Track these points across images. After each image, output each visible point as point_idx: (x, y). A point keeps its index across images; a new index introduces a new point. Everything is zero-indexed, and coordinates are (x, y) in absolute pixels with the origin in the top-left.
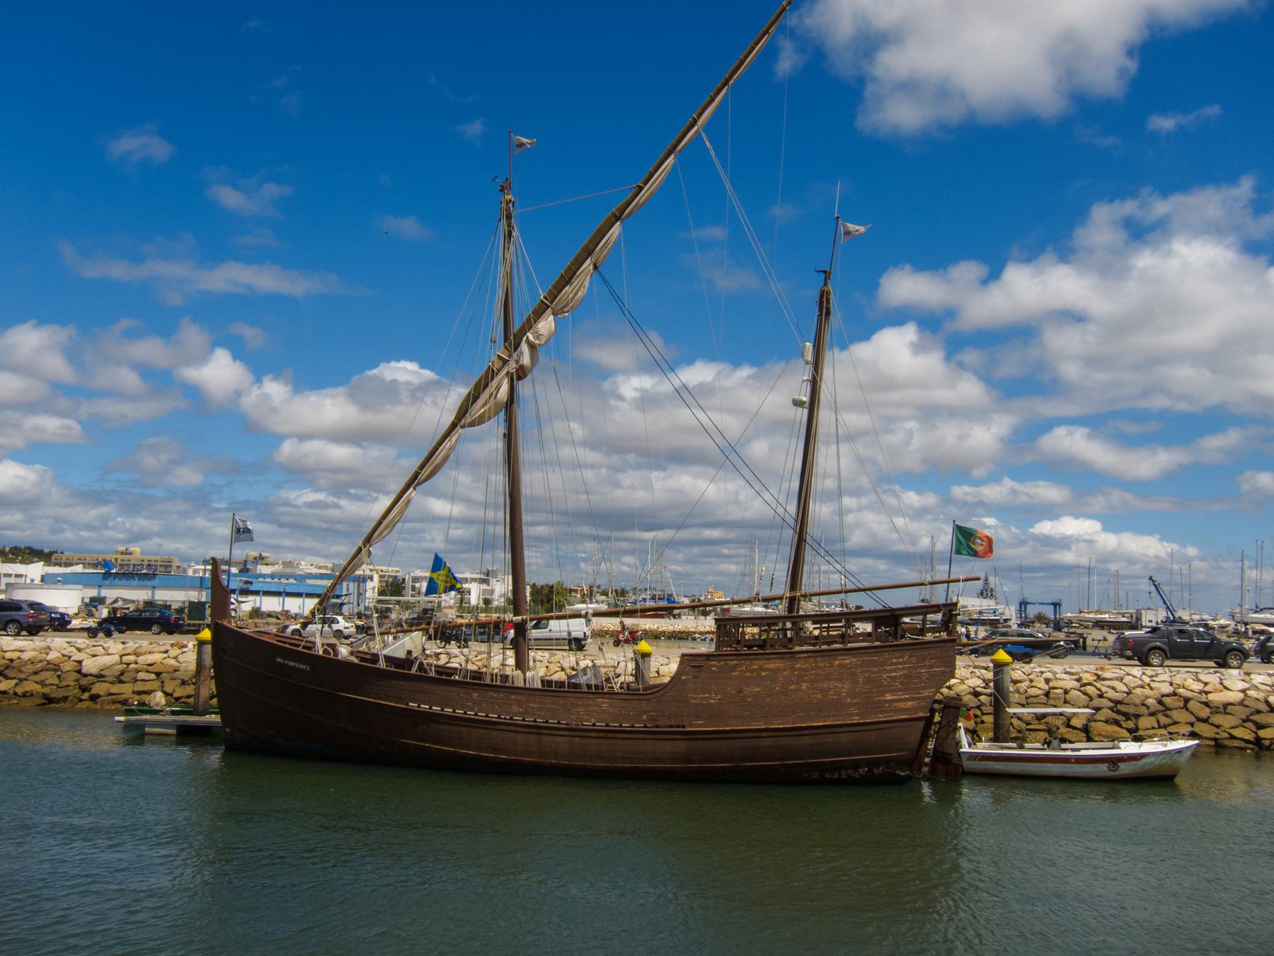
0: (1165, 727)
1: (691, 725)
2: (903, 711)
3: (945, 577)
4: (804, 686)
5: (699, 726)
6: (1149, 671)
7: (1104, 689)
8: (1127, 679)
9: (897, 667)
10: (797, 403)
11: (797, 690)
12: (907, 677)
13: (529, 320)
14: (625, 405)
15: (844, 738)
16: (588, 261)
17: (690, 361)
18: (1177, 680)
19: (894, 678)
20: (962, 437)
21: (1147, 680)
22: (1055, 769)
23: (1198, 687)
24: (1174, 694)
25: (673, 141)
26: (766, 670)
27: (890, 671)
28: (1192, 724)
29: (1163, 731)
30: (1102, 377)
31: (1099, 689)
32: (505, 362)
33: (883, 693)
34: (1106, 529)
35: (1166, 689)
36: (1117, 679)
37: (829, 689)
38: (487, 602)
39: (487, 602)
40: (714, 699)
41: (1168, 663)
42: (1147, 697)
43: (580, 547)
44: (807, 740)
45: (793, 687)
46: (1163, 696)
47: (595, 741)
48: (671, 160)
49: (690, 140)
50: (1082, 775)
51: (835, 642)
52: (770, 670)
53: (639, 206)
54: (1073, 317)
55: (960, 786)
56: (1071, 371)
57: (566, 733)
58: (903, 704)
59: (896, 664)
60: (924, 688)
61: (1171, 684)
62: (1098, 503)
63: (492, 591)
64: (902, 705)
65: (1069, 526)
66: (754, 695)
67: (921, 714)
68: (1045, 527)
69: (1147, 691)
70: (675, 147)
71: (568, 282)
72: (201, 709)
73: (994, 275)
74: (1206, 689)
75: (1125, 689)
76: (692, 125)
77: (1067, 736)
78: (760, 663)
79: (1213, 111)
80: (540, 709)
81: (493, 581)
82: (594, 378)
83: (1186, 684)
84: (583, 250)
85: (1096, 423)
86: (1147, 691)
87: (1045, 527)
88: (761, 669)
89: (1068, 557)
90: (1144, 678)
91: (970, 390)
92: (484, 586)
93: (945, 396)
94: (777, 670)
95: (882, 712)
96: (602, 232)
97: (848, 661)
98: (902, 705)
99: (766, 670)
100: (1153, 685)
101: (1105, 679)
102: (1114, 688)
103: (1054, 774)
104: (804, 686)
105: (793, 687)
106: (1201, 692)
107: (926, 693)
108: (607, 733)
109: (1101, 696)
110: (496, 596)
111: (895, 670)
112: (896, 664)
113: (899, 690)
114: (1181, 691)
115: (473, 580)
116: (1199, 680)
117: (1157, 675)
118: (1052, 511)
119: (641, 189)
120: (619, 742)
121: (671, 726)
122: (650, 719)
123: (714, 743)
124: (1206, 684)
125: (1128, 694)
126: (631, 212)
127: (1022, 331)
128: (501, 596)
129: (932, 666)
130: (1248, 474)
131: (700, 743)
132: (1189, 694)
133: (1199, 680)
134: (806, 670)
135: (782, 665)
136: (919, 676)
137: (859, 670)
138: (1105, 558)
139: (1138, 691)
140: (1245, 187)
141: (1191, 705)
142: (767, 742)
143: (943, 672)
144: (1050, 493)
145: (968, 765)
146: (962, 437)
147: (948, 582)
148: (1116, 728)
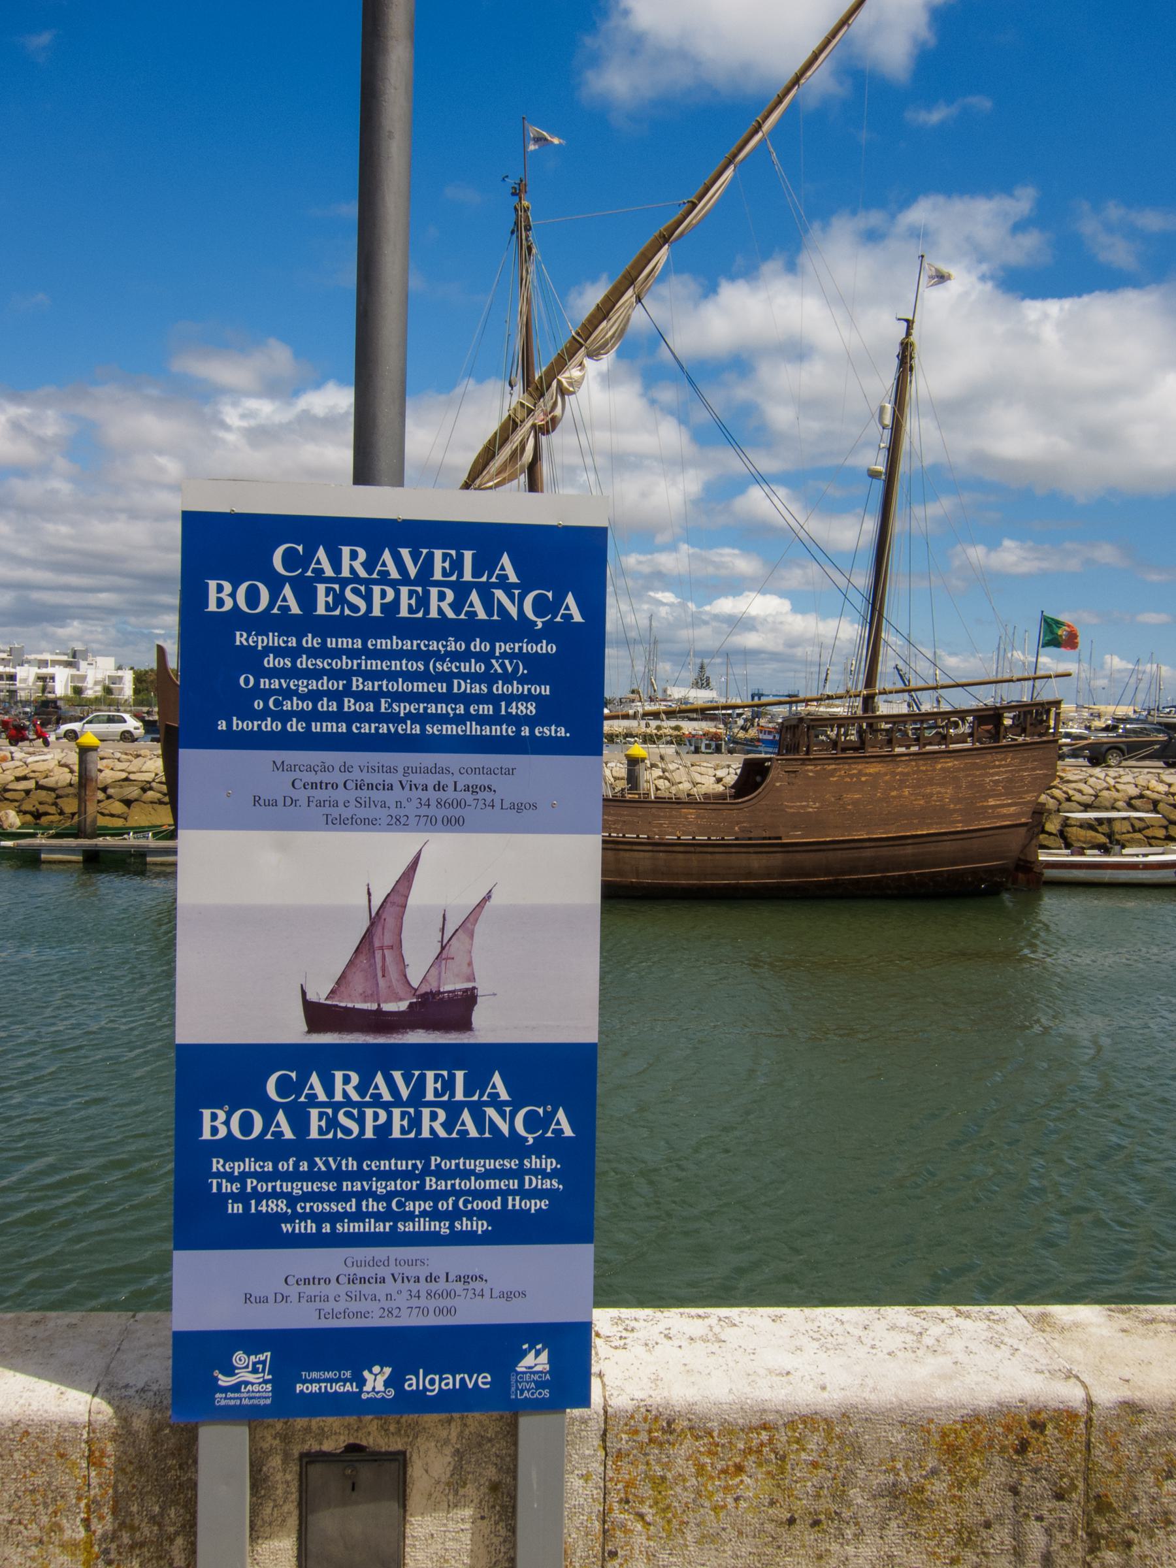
0: (1140, 831)
1: (788, 837)
2: (1005, 817)
3: (1032, 675)
4: (906, 792)
5: (796, 837)
6: (1112, 772)
7: (1071, 792)
8: (1092, 781)
9: (1000, 769)
10: (873, 474)
11: (900, 797)
12: (1009, 780)
13: (560, 356)
14: (230, 437)
15: (948, 847)
16: (630, 292)
17: (318, 385)
18: (1141, 781)
19: (996, 782)
20: (644, 495)
21: (1112, 782)
22: (1107, 875)
23: (1163, 788)
24: (1141, 796)
25: (733, 149)
26: (866, 775)
27: (993, 775)
28: (1166, 828)
29: (1138, 836)
30: (815, 426)
31: (1065, 792)
32: (530, 411)
33: (986, 798)
34: (797, 609)
35: (1134, 792)
36: (1080, 780)
37: (931, 795)
38: (78, 691)
39: (78, 691)
40: (812, 807)
41: (1124, 763)
42: (1116, 800)
43: (155, 621)
44: (909, 850)
45: (894, 793)
46: (1131, 798)
47: (681, 856)
48: (729, 173)
49: (754, 148)
50: (1135, 881)
51: (930, 744)
52: (870, 775)
53: (692, 228)
54: (796, 350)
55: (1040, 898)
56: (781, 416)
57: (650, 848)
58: (1007, 810)
59: (999, 766)
60: (1027, 792)
61: (1136, 786)
62: (795, 577)
63: (83, 678)
64: (1005, 811)
65: (760, 605)
66: (855, 803)
67: (1023, 820)
68: (726, 605)
69: (1114, 794)
70: (735, 156)
71: (605, 317)
72: (89, 830)
73: (710, 290)
74: (1172, 790)
75: (1092, 792)
76: (756, 132)
77: (1045, 843)
78: (860, 767)
79: (982, 103)
80: (615, 822)
81: (83, 664)
82: (199, 399)
83: (1151, 786)
84: (624, 277)
85: (792, 480)
86: (1114, 794)
87: (726, 605)
88: (860, 774)
89: (752, 640)
90: (1108, 779)
91: (669, 435)
92: (73, 671)
93: (641, 441)
94: (877, 775)
95: (985, 818)
96: (646, 257)
97: (950, 763)
98: (1005, 811)
99: (866, 775)
100: (1119, 786)
101: (1069, 781)
102: (1080, 791)
103: (1121, 880)
104: (906, 792)
105: (894, 793)
106: (1167, 794)
107: (1029, 797)
108: (693, 847)
109: (1069, 799)
110: (89, 683)
111: (997, 774)
112: (999, 766)
113: (1001, 795)
114: (1148, 792)
115: (55, 663)
116: (1162, 782)
117: (1120, 776)
118: (735, 586)
119: (694, 205)
120: (709, 857)
121: (764, 838)
122: (742, 830)
123: (812, 855)
124: (1170, 785)
125: (1096, 796)
126: (682, 234)
127: (739, 363)
128: (96, 683)
129: (1034, 769)
130: (959, 548)
131: (799, 856)
132: (1155, 796)
133: (1162, 782)
134: (908, 774)
135: (883, 770)
136: (1022, 779)
137: (961, 774)
138: (793, 643)
139: (1105, 793)
140: (1022, 202)
141: (1161, 806)
142: (868, 853)
143: (1046, 775)
144: (743, 564)
145: (1050, 873)
146: (644, 495)
147: (1035, 679)
148: (1091, 833)
